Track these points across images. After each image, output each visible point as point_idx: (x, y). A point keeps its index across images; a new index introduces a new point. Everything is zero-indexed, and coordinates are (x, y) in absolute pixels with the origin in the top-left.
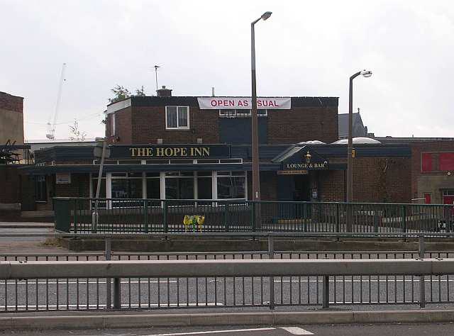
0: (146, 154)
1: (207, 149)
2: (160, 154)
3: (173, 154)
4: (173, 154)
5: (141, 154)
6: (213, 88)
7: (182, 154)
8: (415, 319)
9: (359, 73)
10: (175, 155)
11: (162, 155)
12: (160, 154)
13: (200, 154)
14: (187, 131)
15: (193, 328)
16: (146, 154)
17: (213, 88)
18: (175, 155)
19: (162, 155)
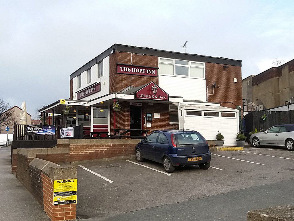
0: (127, 70)
1: (154, 71)
2: (134, 71)
3: (139, 72)
4: (139, 72)
5: (126, 70)
6: (187, 42)
7: (143, 72)
8: (90, 75)
9: (182, 97)
10: (140, 72)
11: (135, 72)
12: (134, 71)
13: (151, 73)
14: (141, 106)
15: (41, 187)
16: (127, 70)
17: (187, 42)
18: (140, 72)
19: (135, 72)
